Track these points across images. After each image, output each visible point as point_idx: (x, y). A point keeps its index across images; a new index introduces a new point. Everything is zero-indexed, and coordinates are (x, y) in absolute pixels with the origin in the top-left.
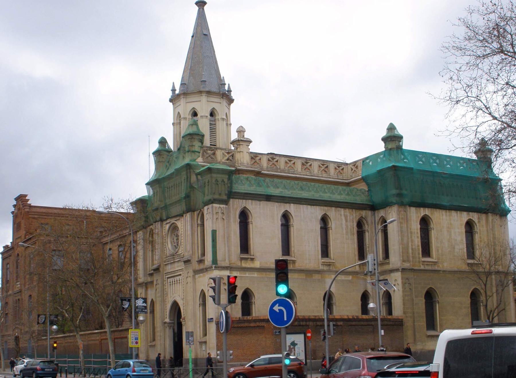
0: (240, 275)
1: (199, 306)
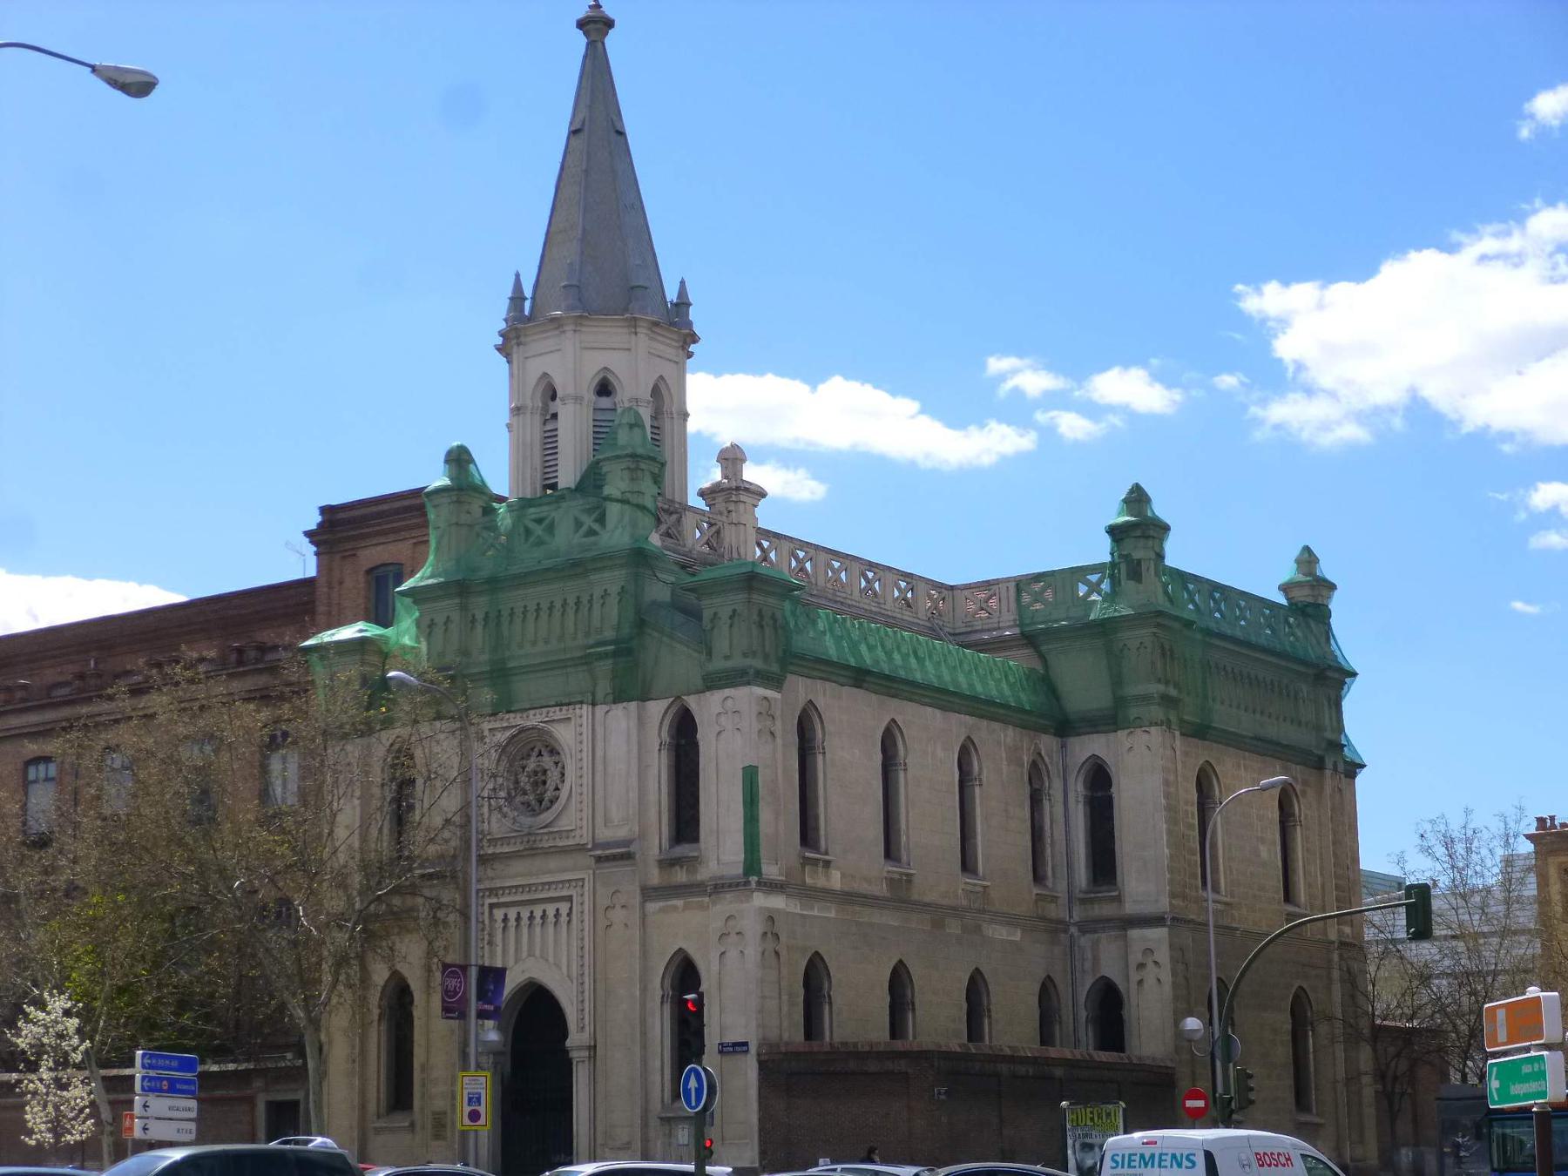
1: (662, 1003)
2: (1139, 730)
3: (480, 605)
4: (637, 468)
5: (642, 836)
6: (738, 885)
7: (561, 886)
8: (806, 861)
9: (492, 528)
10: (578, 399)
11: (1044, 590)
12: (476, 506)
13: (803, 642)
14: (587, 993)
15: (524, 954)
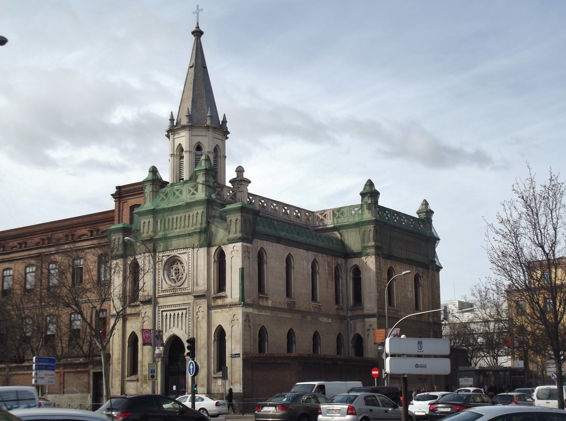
6: (237, 305)
8: (260, 297)
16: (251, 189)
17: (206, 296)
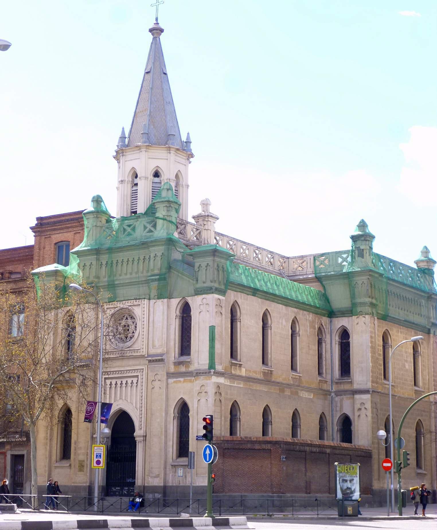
0: (236, 385)
2: (361, 316)
3: (104, 258)
4: (170, 206)
5: (168, 352)
7: (134, 371)
8: (232, 364)
9: (110, 228)
10: (146, 178)
11: (325, 259)
12: (104, 219)
13: (235, 277)
14: (143, 415)
15: (118, 398)
16: (219, 227)
17: (165, 361)
